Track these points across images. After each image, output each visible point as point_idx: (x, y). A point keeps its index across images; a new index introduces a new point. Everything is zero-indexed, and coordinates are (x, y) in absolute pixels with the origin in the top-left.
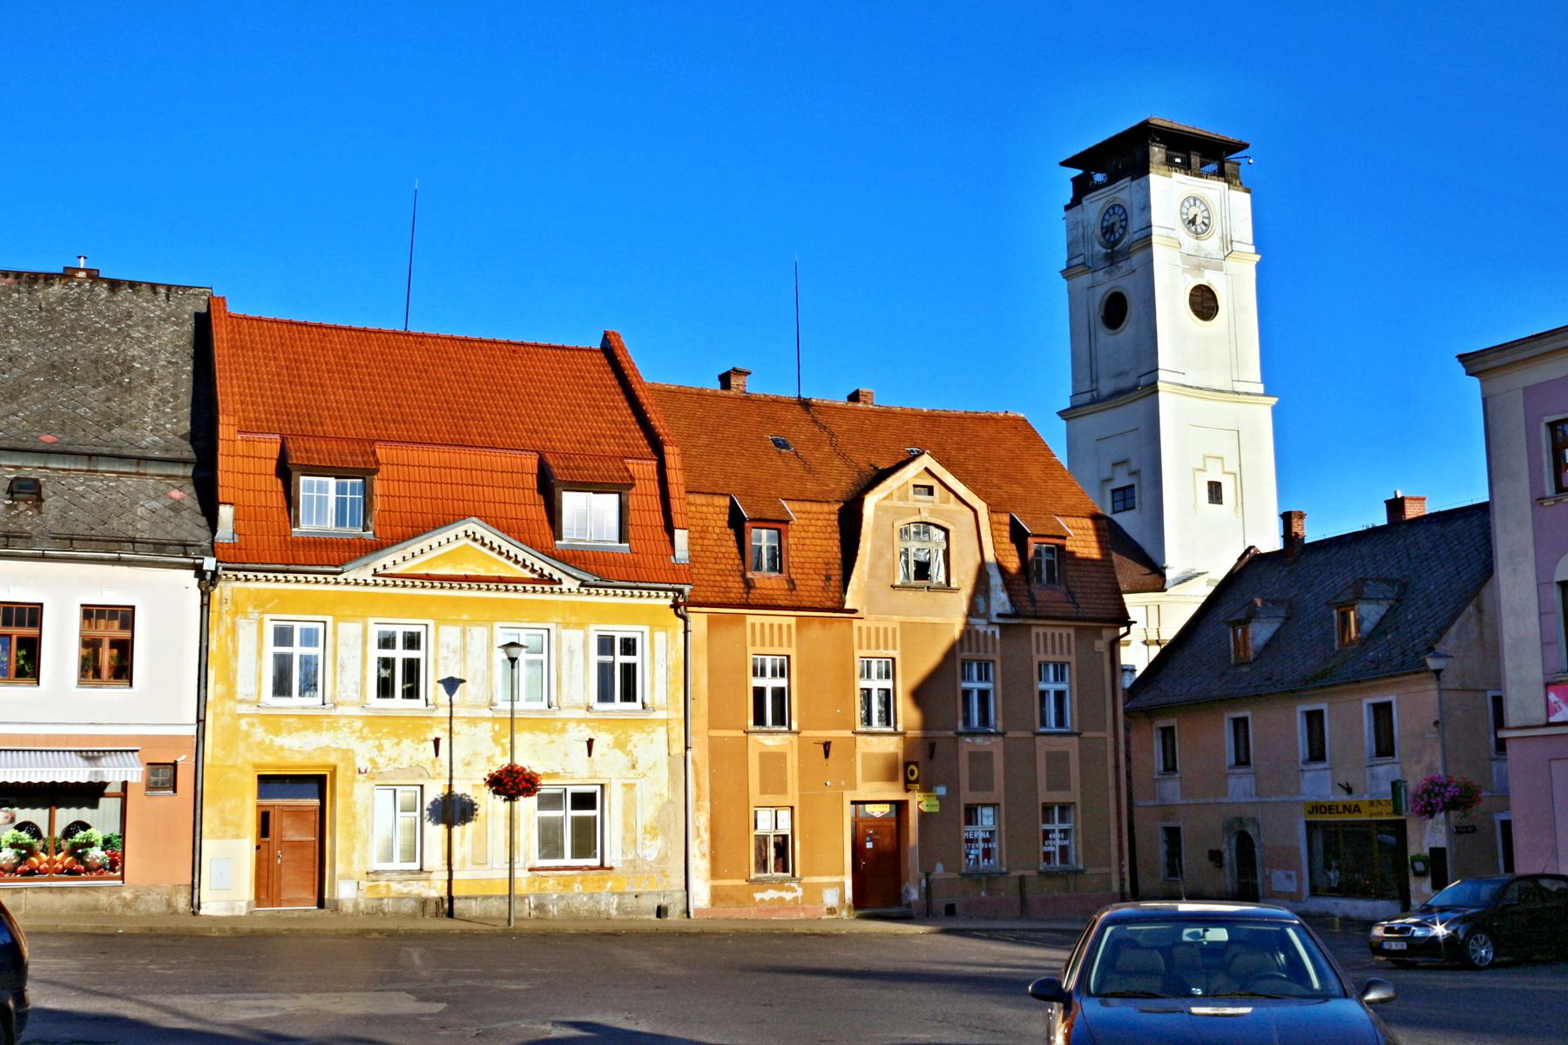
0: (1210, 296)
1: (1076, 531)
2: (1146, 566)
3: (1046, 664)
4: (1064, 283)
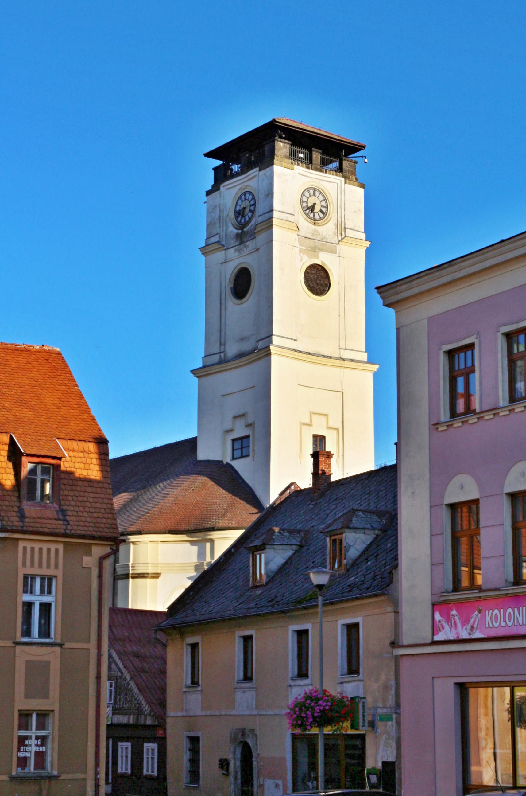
0: (324, 275)
1: (71, 454)
2: (255, 507)
3: (33, 578)
4: (203, 258)
